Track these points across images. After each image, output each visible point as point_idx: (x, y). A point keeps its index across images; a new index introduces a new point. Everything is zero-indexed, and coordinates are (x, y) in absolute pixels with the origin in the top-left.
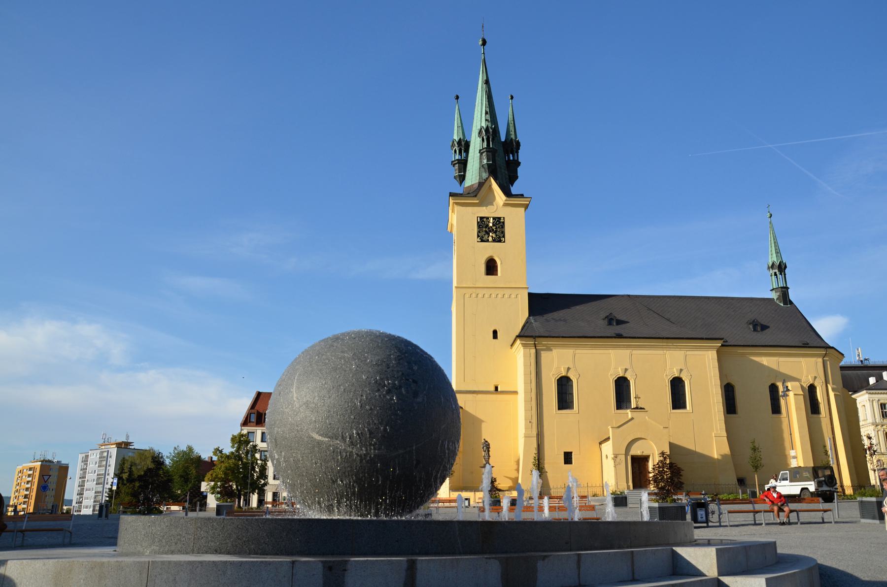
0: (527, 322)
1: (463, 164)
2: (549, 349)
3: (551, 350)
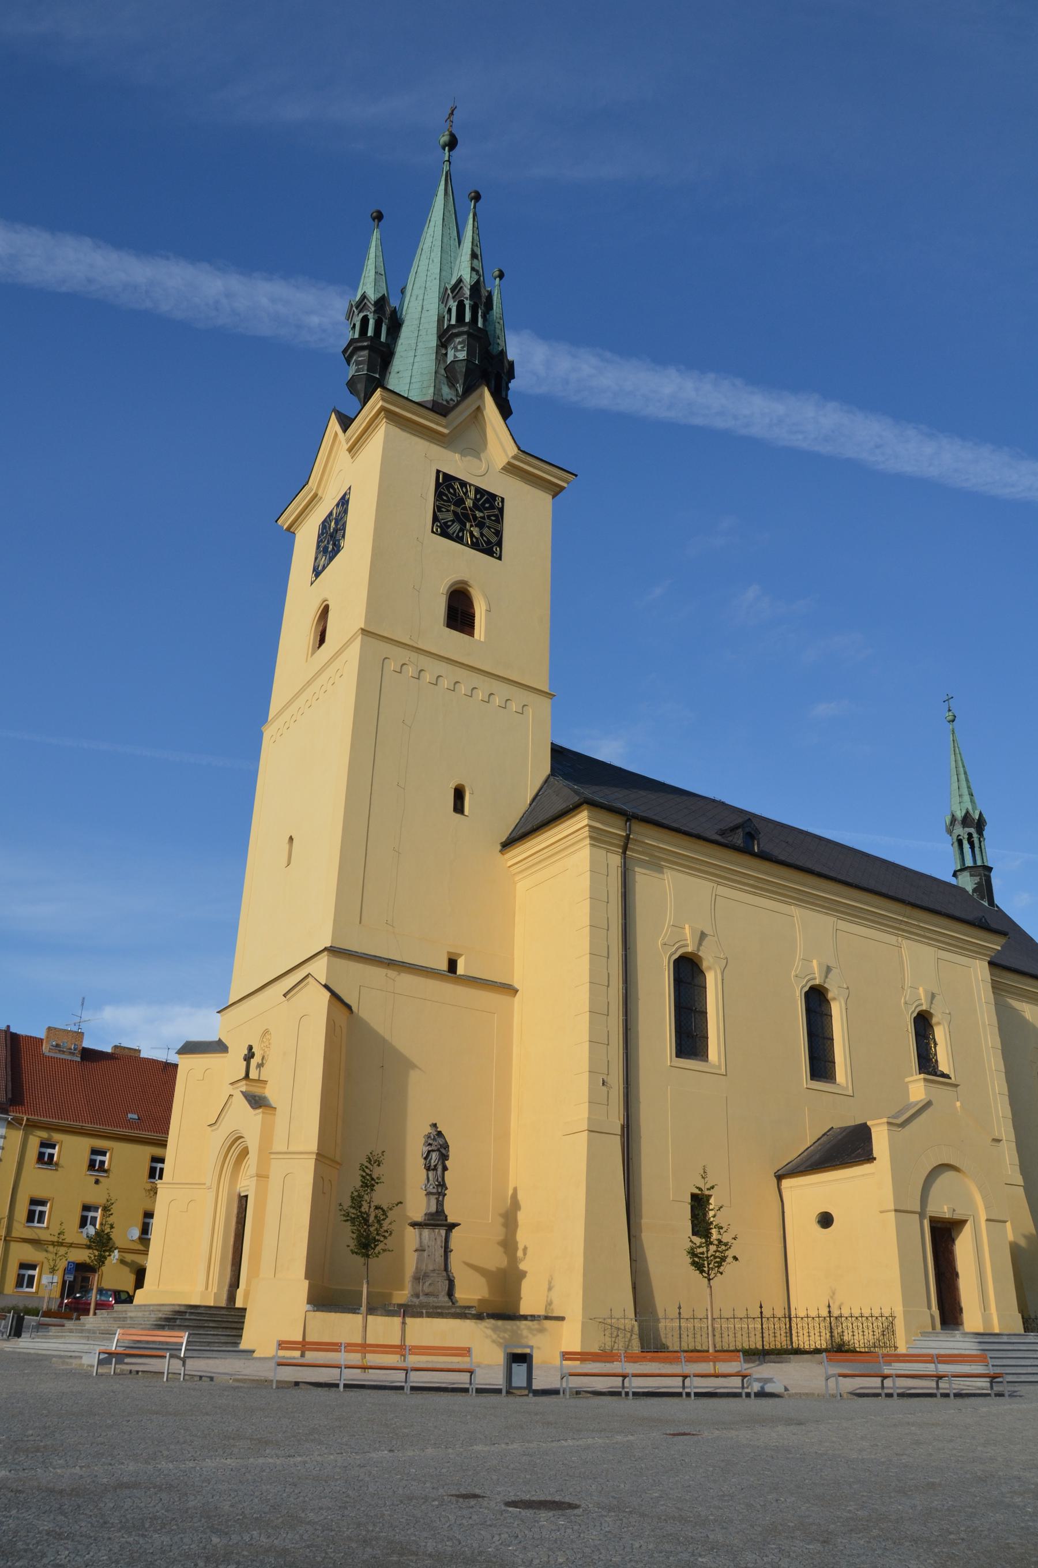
2: (656, 865)
3: (660, 869)
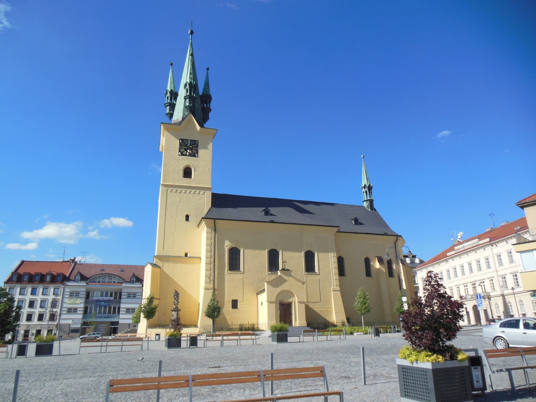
0: (209, 210)
1: (172, 106)
